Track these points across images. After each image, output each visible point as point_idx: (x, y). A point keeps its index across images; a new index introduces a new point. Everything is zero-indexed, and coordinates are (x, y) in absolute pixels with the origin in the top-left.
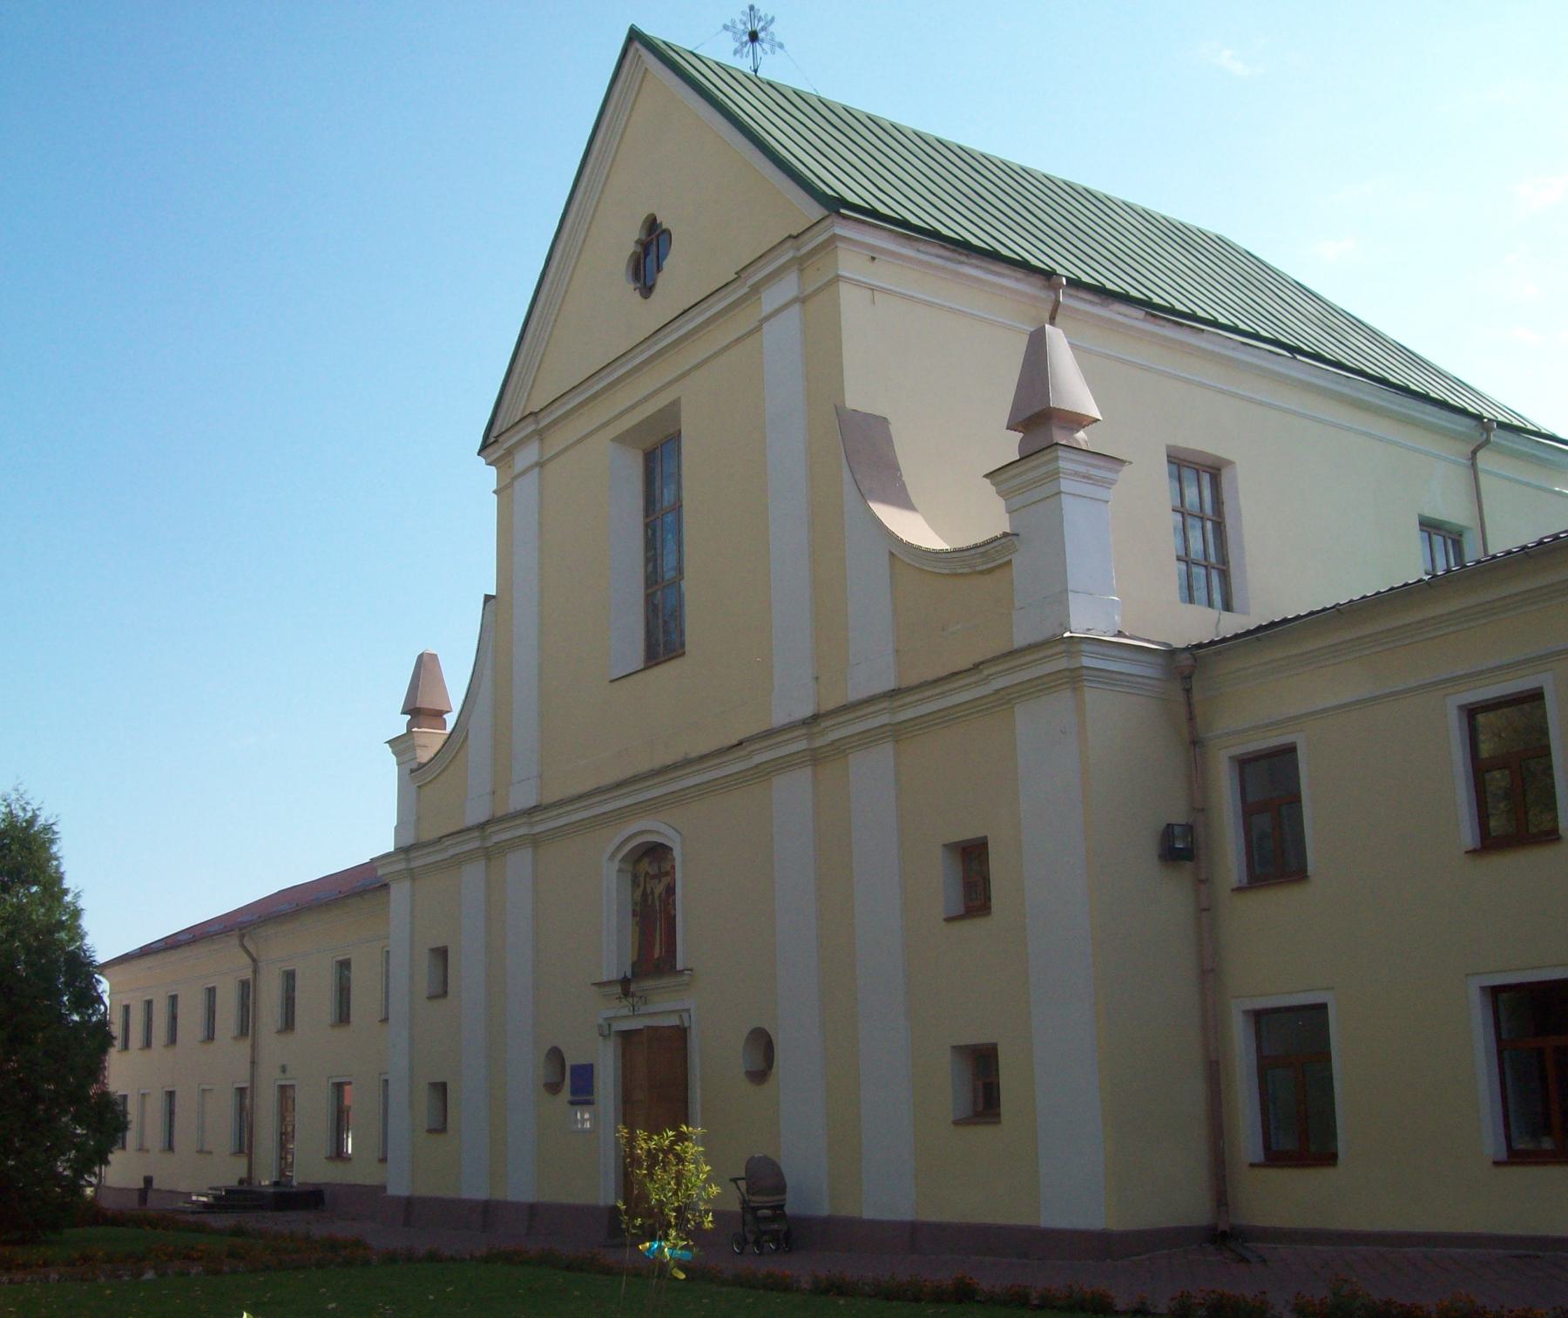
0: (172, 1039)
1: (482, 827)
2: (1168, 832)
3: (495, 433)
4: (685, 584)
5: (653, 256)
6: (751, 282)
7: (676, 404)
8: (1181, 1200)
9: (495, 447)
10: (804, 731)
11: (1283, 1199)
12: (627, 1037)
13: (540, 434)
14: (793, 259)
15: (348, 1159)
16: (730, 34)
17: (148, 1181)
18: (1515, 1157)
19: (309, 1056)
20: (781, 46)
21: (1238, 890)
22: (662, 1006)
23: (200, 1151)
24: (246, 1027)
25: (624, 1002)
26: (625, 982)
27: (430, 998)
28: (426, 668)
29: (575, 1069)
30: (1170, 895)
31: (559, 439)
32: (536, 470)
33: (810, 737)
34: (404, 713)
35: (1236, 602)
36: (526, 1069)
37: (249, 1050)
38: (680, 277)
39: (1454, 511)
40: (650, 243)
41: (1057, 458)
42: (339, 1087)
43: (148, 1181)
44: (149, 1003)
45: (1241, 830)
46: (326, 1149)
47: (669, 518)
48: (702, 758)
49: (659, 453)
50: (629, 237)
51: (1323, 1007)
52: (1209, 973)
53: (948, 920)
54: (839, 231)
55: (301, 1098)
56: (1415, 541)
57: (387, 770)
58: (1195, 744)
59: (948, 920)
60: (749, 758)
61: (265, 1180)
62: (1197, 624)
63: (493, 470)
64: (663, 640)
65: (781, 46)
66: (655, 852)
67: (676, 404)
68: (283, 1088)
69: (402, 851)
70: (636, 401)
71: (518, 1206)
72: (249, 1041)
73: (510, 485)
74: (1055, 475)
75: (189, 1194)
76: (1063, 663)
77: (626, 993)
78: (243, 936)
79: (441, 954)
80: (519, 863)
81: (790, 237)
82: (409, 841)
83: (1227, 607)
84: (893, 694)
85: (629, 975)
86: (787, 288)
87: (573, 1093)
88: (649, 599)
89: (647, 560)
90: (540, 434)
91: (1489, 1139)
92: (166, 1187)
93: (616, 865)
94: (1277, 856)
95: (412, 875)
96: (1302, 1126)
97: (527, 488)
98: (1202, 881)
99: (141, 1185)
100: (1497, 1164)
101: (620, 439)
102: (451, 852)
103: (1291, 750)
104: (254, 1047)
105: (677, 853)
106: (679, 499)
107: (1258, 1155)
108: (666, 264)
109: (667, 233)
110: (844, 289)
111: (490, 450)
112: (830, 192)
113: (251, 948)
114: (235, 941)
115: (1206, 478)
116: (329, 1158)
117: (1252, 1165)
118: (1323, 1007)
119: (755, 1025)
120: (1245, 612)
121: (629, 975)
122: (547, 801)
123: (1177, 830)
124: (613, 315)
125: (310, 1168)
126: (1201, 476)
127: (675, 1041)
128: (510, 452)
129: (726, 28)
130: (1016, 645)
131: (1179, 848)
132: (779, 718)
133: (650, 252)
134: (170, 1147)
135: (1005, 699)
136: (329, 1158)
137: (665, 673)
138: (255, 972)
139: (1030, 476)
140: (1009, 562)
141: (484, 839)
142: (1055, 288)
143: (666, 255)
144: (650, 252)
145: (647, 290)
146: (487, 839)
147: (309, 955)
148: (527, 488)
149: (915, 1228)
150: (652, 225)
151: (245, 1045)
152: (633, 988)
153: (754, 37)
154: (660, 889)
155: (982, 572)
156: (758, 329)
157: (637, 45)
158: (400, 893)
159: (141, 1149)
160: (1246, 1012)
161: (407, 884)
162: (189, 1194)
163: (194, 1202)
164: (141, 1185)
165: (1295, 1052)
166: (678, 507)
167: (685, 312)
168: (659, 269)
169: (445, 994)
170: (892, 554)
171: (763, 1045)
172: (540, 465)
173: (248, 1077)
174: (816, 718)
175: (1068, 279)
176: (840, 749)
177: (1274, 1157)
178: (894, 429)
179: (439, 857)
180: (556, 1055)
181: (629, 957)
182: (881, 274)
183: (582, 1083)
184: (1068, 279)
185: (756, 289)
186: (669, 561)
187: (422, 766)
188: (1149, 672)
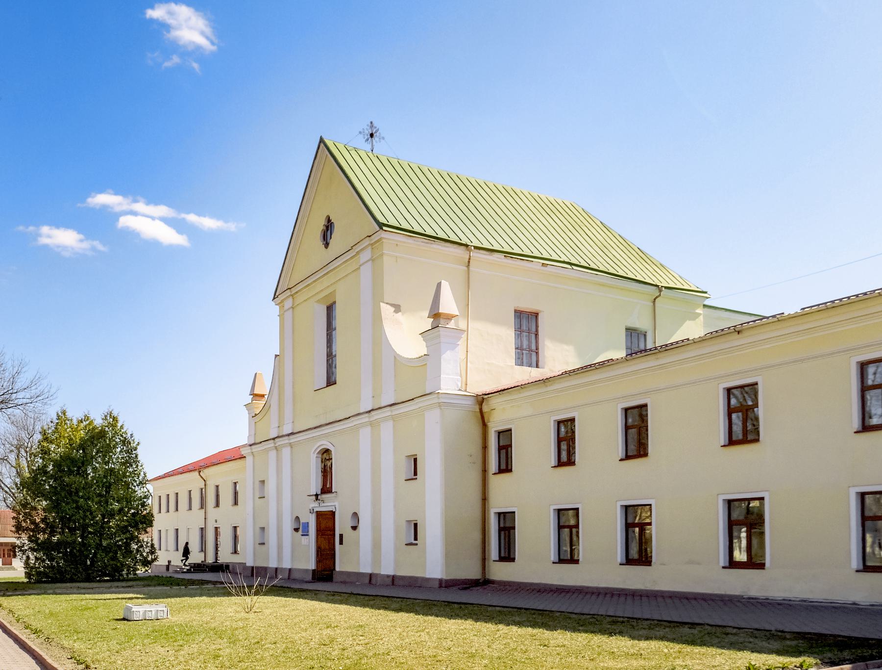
11: (500, 572)
16: (361, 136)
17: (169, 562)
19: (224, 517)
20: (383, 138)
22: (328, 504)
24: (203, 505)
26: (317, 495)
33: (369, 417)
35: (540, 364)
36: (288, 525)
38: (336, 239)
39: (642, 323)
43: (169, 562)
46: (230, 549)
54: (383, 236)
55: (221, 531)
57: (245, 415)
58: (484, 425)
61: (210, 560)
63: (278, 307)
65: (383, 138)
66: (327, 451)
68: (216, 528)
72: (495, 426)
74: (439, 336)
76: (436, 401)
83: (537, 366)
100: (723, 567)
110: (385, 258)
124: (314, 253)
125: (225, 557)
129: (360, 133)
142: (470, 251)
145: (327, 245)
148: (289, 314)
149: (394, 578)
150: (329, 220)
153: (372, 135)
154: (329, 464)
156: (359, 268)
165: (507, 525)
177: (502, 559)
181: (320, 487)
187: (256, 415)
188: (469, 403)
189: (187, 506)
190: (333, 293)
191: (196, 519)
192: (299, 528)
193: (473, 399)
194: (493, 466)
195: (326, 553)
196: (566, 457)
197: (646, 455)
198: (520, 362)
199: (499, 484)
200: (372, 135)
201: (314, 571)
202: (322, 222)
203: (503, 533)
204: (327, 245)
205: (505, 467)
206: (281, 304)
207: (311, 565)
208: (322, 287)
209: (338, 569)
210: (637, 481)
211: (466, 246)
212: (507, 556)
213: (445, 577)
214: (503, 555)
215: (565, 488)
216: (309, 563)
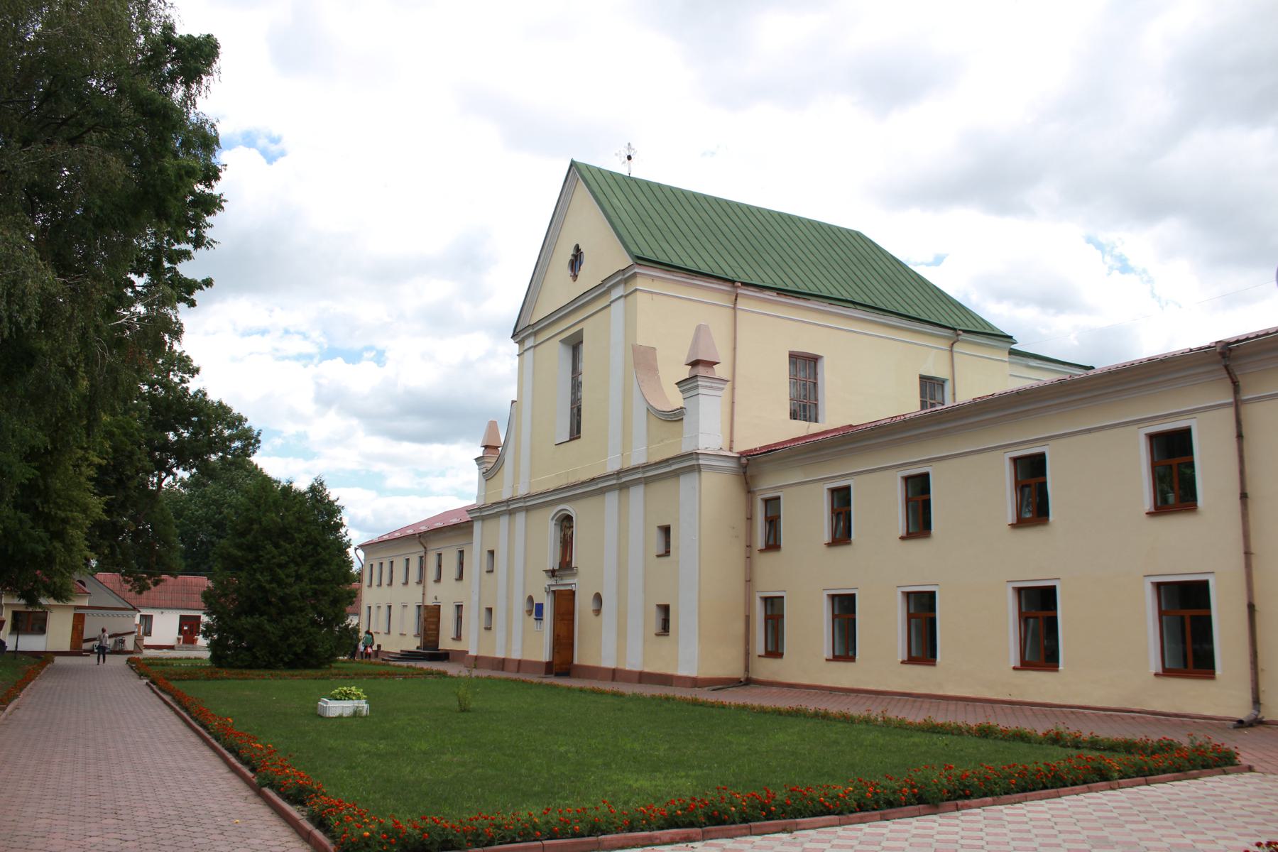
0: (390, 584)
8: (730, 667)
11: (768, 669)
18: (1167, 672)
21: (761, 551)
22: (566, 582)
24: (421, 581)
36: (520, 605)
41: (697, 387)
50: (568, 254)
52: (749, 581)
70: (566, 327)
71: (514, 660)
86: (618, 292)
91: (1154, 663)
100: (1015, 668)
102: (674, 467)
107: (763, 653)
122: (626, 466)
126: (805, 365)
133: (576, 260)
144: (576, 260)
145: (575, 277)
150: (577, 248)
151: (421, 587)
158: (477, 527)
169: (667, 553)
171: (598, 598)
180: (530, 599)
189: (455, 574)
193: (957, 347)
194: (760, 542)
195: (564, 640)
196: (842, 534)
198: (794, 415)
199: (766, 563)
200: (629, 158)
202: (572, 251)
203: (913, 621)
204: (575, 277)
205: (773, 545)
206: (520, 343)
208: (566, 327)
209: (576, 662)
210: (920, 565)
211: (733, 282)
212: (774, 650)
213: (702, 676)
214: (914, 654)
215: (842, 569)
216: (543, 653)
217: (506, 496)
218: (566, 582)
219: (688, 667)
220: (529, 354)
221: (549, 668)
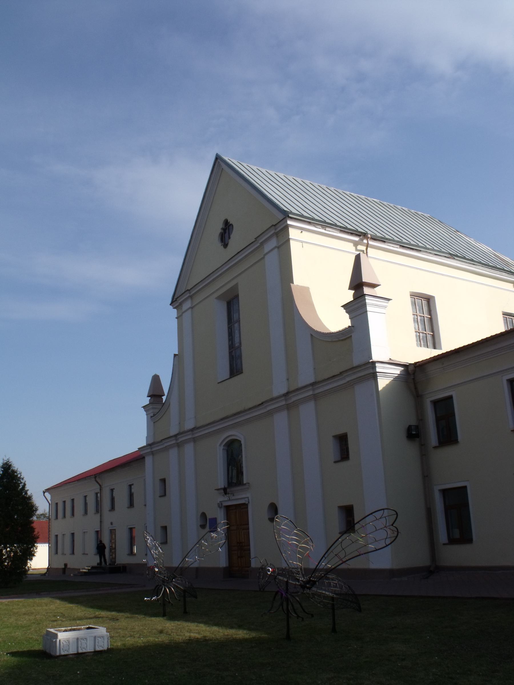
0: (73, 514)
1: (176, 436)
2: (409, 429)
3: (176, 297)
4: (242, 348)
5: (227, 234)
6: (260, 242)
7: (236, 285)
9: (176, 302)
10: (311, 388)
12: (228, 508)
13: (191, 297)
14: (274, 233)
15: (135, 555)
17: (66, 565)
21: (435, 447)
22: (239, 497)
23: (84, 554)
24: (98, 509)
25: (225, 496)
26: (225, 489)
27: (160, 496)
28: (156, 380)
29: (210, 519)
30: (411, 450)
31: (198, 299)
32: (190, 310)
33: (314, 390)
34: (148, 397)
35: (437, 346)
36: (193, 521)
37: (99, 517)
38: (237, 240)
40: (226, 229)
42: (131, 529)
43: (66, 565)
44: (64, 502)
45: (436, 428)
46: (127, 551)
47: (236, 325)
48: (250, 409)
49: (231, 302)
51: (465, 487)
52: (426, 477)
53: (335, 462)
56: (500, 319)
59: (335, 462)
60: (263, 410)
62: (426, 353)
63: (175, 310)
64: (235, 369)
67: (236, 285)
69: (149, 445)
70: (222, 285)
72: (99, 514)
73: (181, 316)
75: (80, 569)
77: (226, 493)
78: (95, 477)
79: (163, 481)
80: (189, 449)
81: (273, 225)
82: (151, 442)
83: (435, 348)
84: (313, 384)
85: (226, 486)
87: (210, 528)
88: (230, 353)
89: (229, 340)
90: (191, 297)
92: (72, 567)
93: (222, 447)
94: (448, 435)
95: (153, 453)
96: (460, 528)
97: (187, 316)
98: (422, 445)
99: (63, 567)
101: (219, 298)
102: (348, 379)
103: (450, 398)
104: (101, 516)
105: (243, 442)
106: (239, 318)
108: (232, 236)
109: (232, 225)
111: (174, 303)
112: (286, 209)
113: (99, 481)
114: (94, 479)
115: (424, 303)
116: (128, 555)
117: (444, 544)
118: (465, 487)
119: (271, 502)
120: (441, 349)
121: (226, 486)
122: (292, 389)
123: (413, 427)
124: (215, 255)
127: (243, 508)
128: (181, 304)
130: (355, 365)
131: (414, 434)
132: (275, 394)
133: (227, 228)
134: (73, 553)
135: (270, 413)
136: (128, 555)
137: (237, 379)
138: (100, 490)
139: (356, 306)
140: (351, 336)
141: (151, 448)
143: (232, 233)
144: (227, 228)
145: (225, 246)
146: (178, 440)
147: (119, 484)
148: (187, 316)
152: (228, 490)
155: (342, 340)
156: (264, 258)
157: (281, 216)
158: (148, 460)
159: (63, 554)
160: (440, 490)
161: (151, 456)
162: (80, 569)
163: (82, 572)
164: (63, 567)
166: (239, 321)
167: (238, 253)
168: (229, 238)
169: (165, 495)
170: (312, 335)
171: (274, 509)
172: (192, 308)
173: (99, 527)
174: (288, 393)
175: (371, 235)
176: (296, 404)
177: (452, 541)
178: (312, 291)
179: (162, 447)
180: (204, 515)
182: (306, 236)
183: (213, 525)
184: (371, 235)
185: (262, 244)
186: (237, 340)
189: (82, 512)
190: (235, 288)
191: (92, 522)
192: (208, 523)
195: (238, 544)
197: (133, 507)
201: (225, 569)
207: (223, 562)
212: (465, 538)
213: (395, 567)
217: (173, 432)
218: (239, 497)
219: (382, 561)
220: (188, 314)
221: (229, 572)
